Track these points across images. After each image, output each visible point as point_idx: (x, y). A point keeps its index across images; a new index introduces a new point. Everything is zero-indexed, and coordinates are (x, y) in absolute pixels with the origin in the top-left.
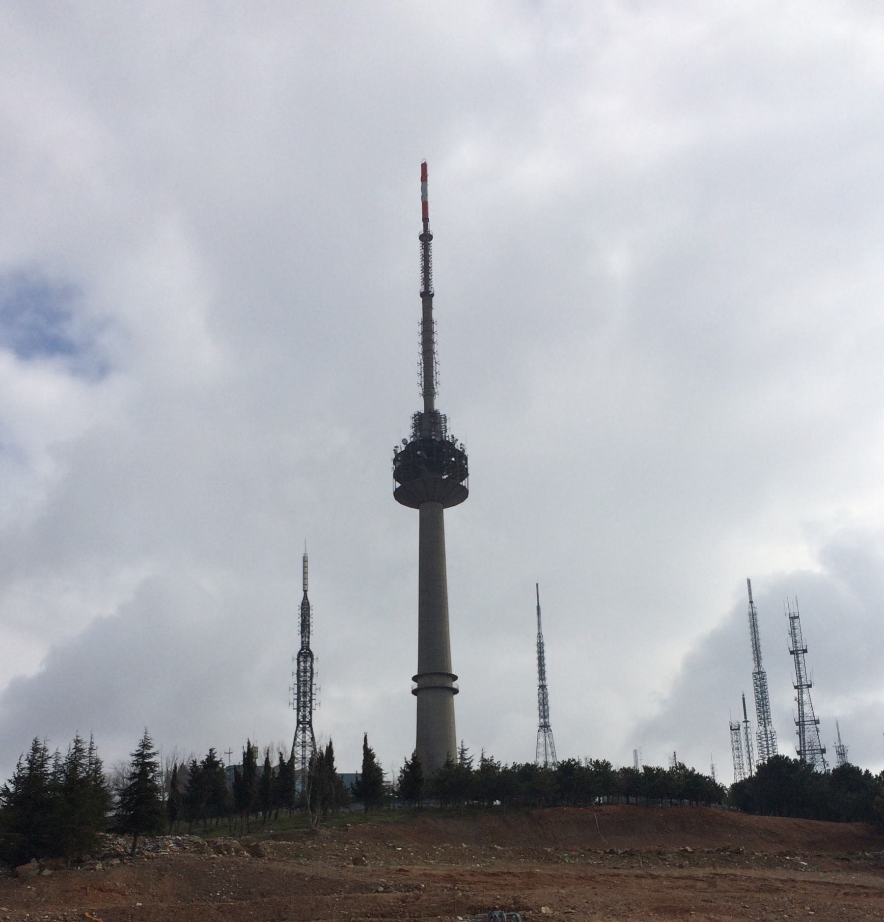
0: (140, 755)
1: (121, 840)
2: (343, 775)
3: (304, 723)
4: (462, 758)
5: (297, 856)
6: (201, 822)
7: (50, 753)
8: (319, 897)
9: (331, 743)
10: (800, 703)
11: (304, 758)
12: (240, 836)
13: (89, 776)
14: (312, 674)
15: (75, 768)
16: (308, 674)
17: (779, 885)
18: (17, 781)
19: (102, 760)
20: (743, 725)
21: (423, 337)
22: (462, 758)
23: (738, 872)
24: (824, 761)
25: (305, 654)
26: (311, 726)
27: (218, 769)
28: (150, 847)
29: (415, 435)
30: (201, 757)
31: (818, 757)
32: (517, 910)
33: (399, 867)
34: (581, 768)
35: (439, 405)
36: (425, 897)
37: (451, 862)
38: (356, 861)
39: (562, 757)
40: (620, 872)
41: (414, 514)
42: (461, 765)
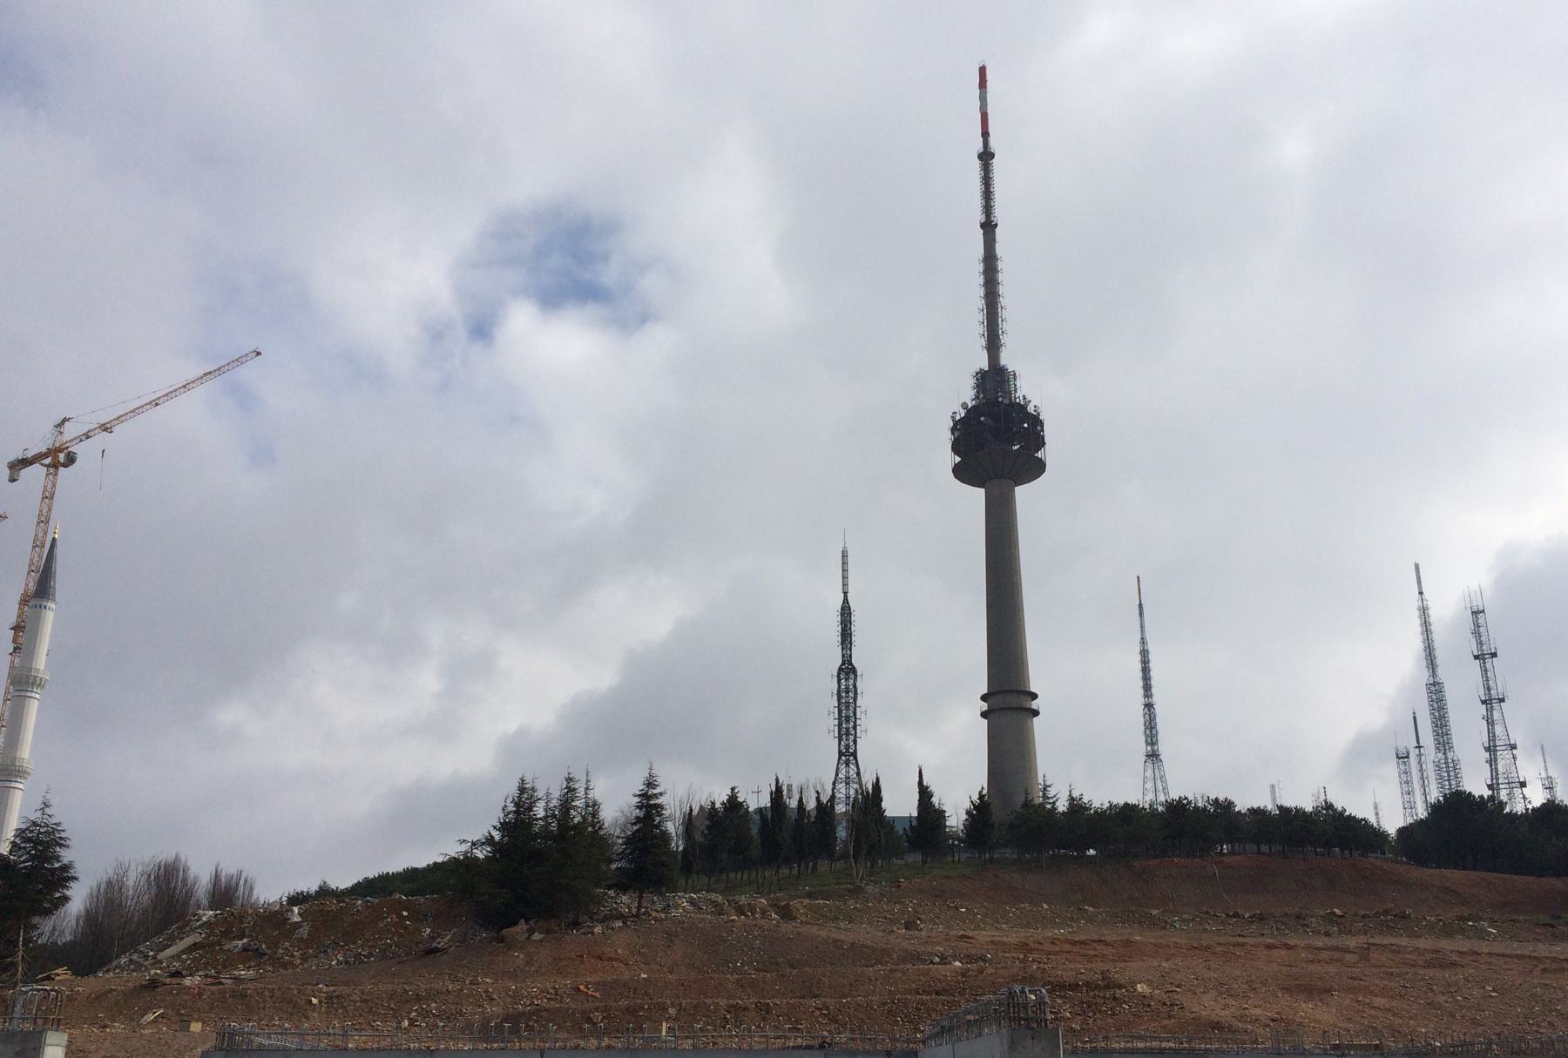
0: (645, 796)
1: (625, 899)
2: (894, 819)
3: (848, 755)
4: (1045, 796)
7: (540, 794)
10: (1490, 722)
11: (848, 798)
17: (1455, 958)
18: (504, 827)
25: (847, 670)
28: (659, 906)
29: (977, 397)
31: (1517, 791)
32: (1107, 987)
34: (1196, 808)
35: (1007, 359)
37: (1028, 925)
39: (1175, 795)
41: (979, 494)
42: (1042, 805)
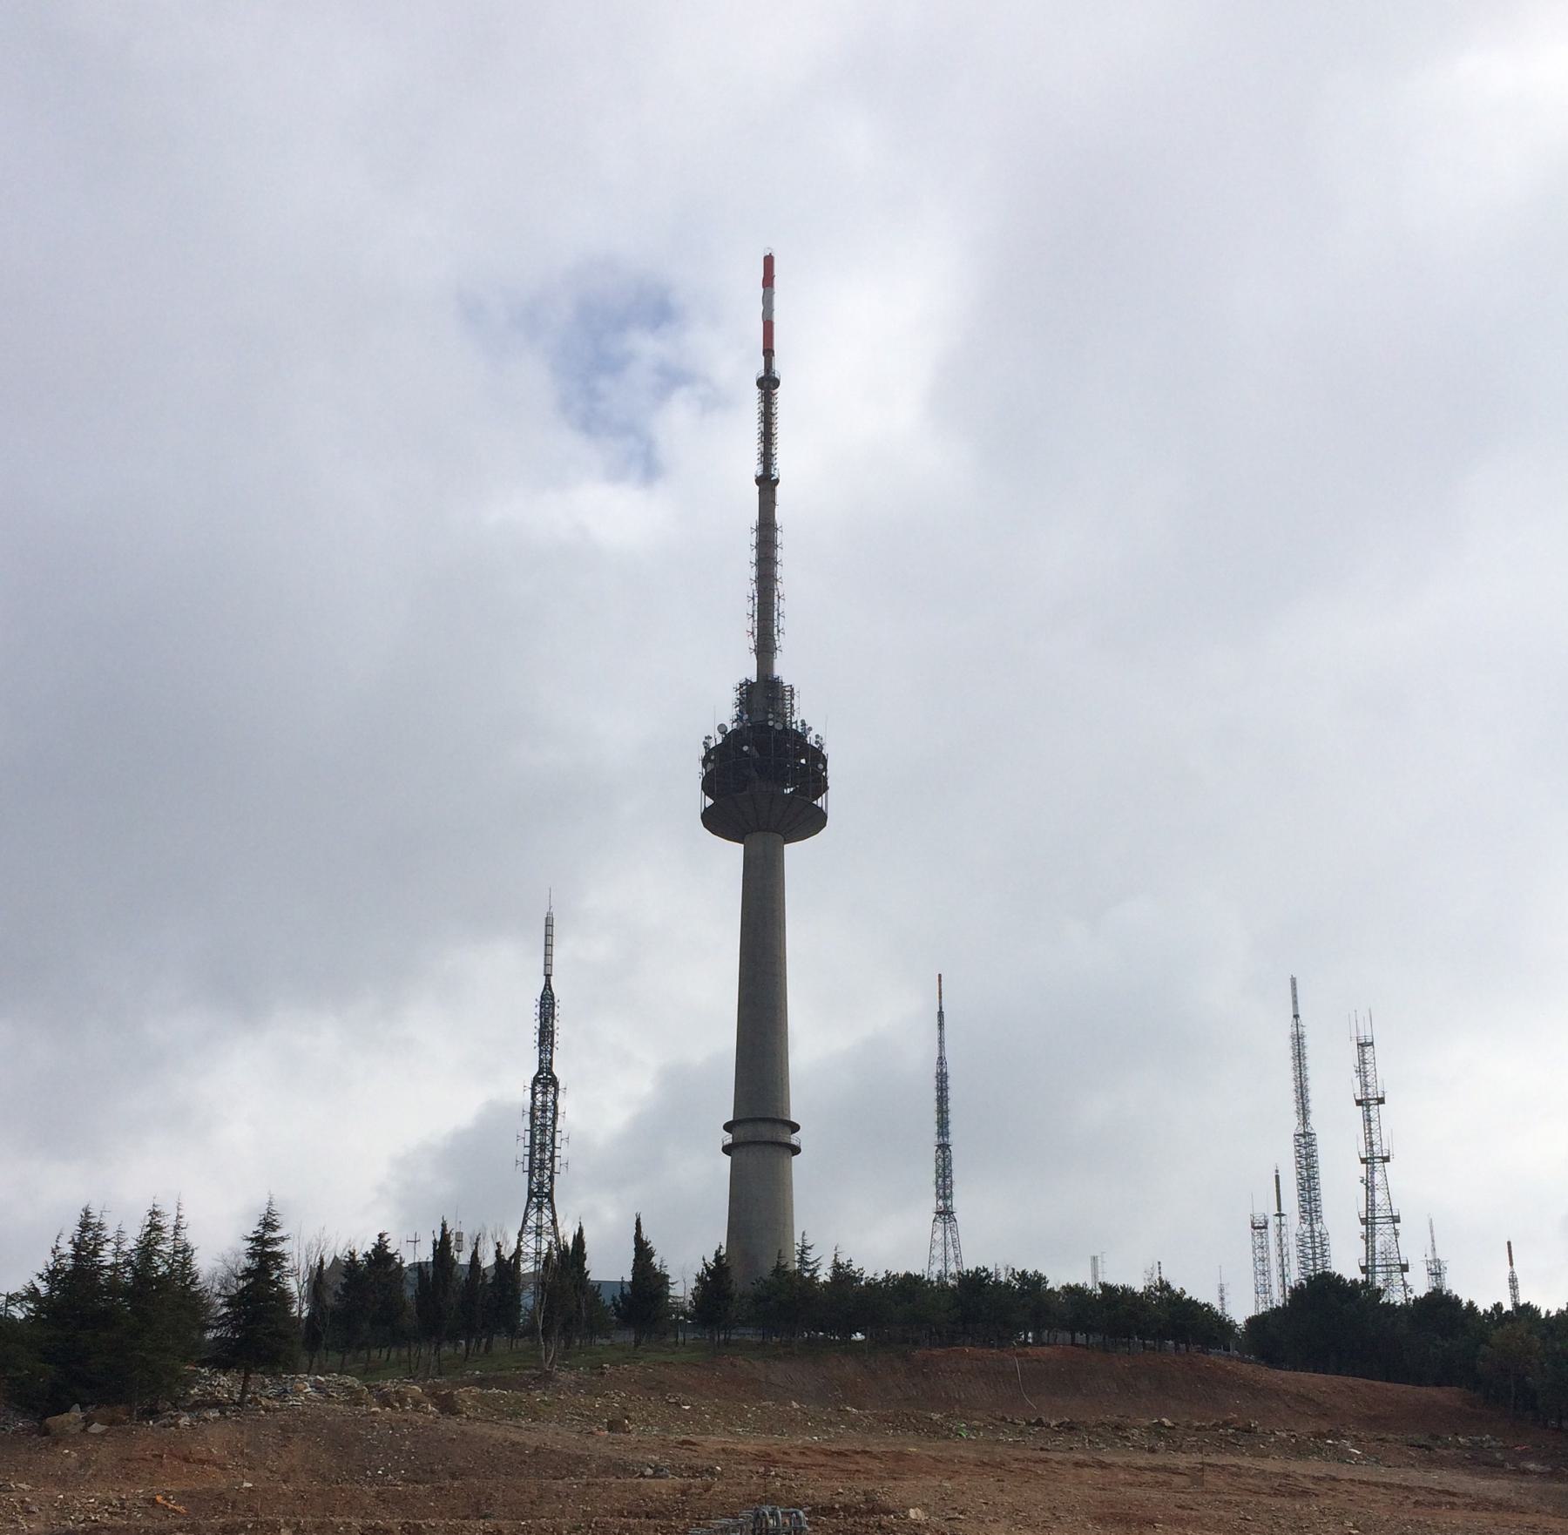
0: (259, 1240)
1: (224, 1380)
2: (600, 1284)
4: (802, 1260)
5: (515, 1415)
6: (363, 1354)
7: (110, 1233)
8: (545, 1483)
9: (581, 1230)
10: (1370, 1187)
12: (425, 1379)
13: (172, 1272)
14: (555, 1113)
15: (149, 1259)
16: (549, 1115)
18: (52, 1276)
19: (193, 1246)
20: (1273, 1223)
21: (759, 554)
22: (802, 1260)
23: (1245, 1462)
24: (1405, 1285)
26: (551, 1201)
27: (393, 1267)
28: (270, 1391)
29: (739, 718)
30: (365, 1247)
31: (1396, 1277)
32: (871, 1512)
33: (684, 1437)
35: (782, 669)
36: (719, 1487)
37: (771, 1431)
38: (613, 1426)
39: (970, 1265)
40: (1050, 1456)
41: (731, 855)
